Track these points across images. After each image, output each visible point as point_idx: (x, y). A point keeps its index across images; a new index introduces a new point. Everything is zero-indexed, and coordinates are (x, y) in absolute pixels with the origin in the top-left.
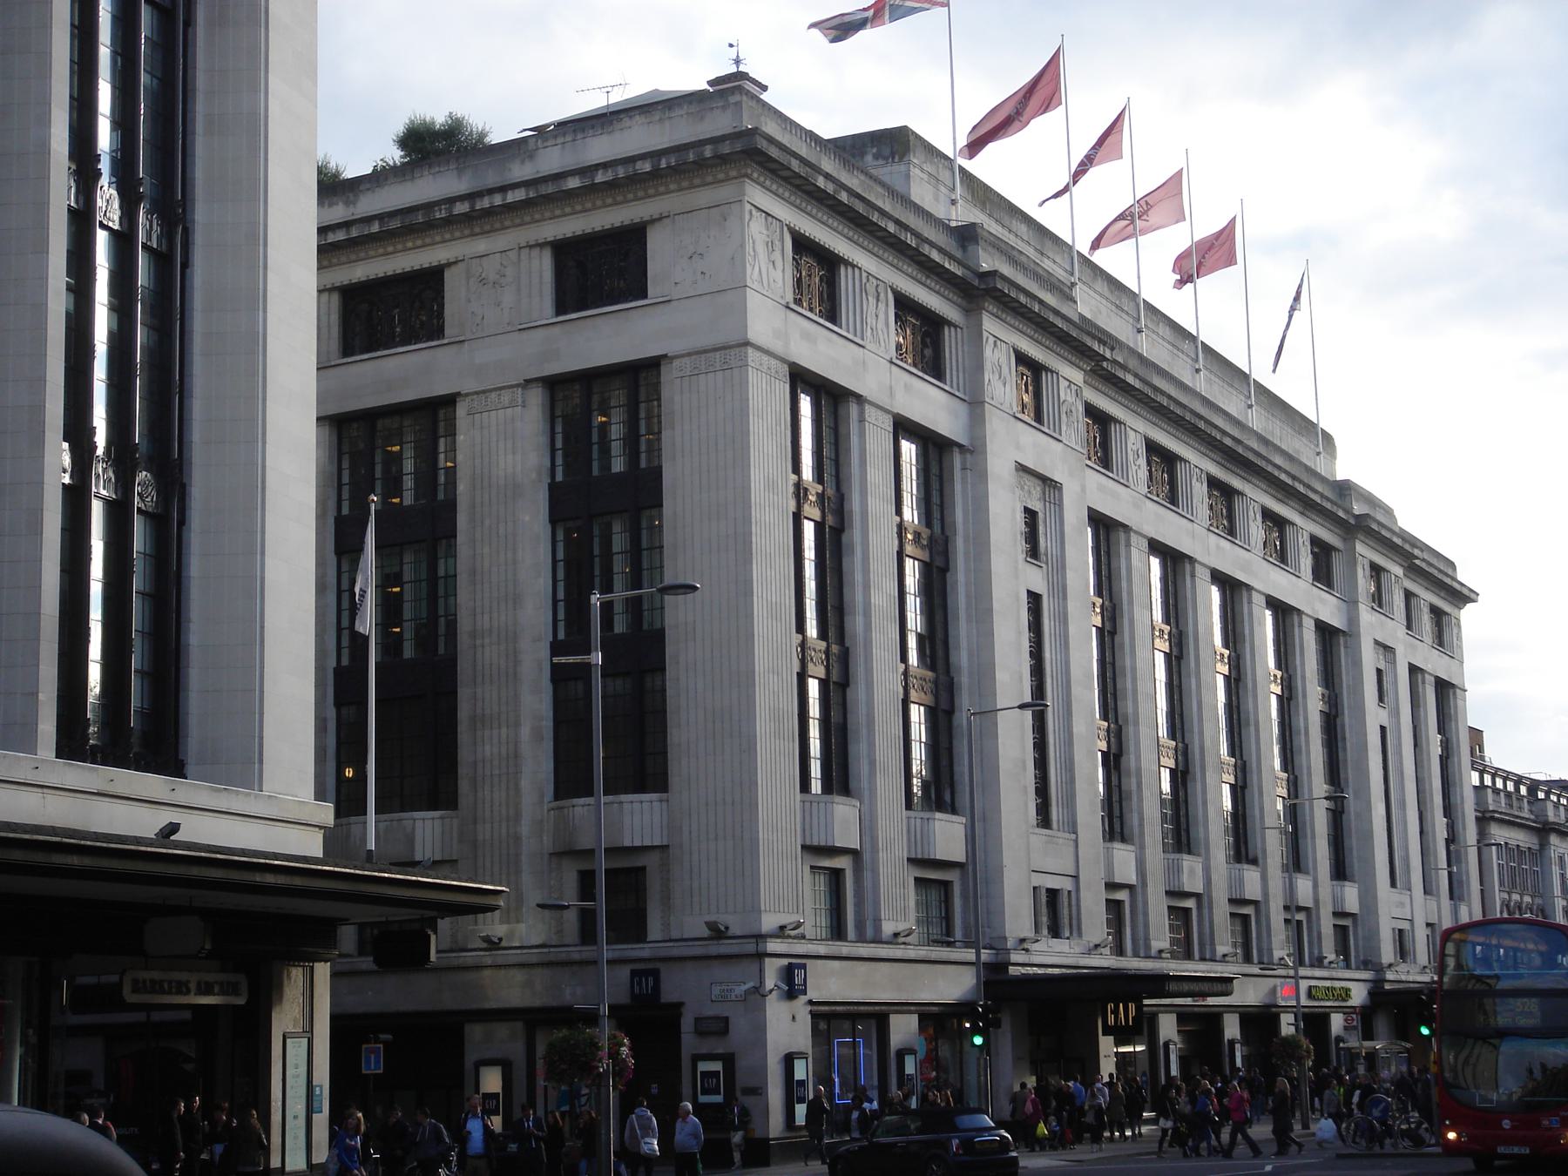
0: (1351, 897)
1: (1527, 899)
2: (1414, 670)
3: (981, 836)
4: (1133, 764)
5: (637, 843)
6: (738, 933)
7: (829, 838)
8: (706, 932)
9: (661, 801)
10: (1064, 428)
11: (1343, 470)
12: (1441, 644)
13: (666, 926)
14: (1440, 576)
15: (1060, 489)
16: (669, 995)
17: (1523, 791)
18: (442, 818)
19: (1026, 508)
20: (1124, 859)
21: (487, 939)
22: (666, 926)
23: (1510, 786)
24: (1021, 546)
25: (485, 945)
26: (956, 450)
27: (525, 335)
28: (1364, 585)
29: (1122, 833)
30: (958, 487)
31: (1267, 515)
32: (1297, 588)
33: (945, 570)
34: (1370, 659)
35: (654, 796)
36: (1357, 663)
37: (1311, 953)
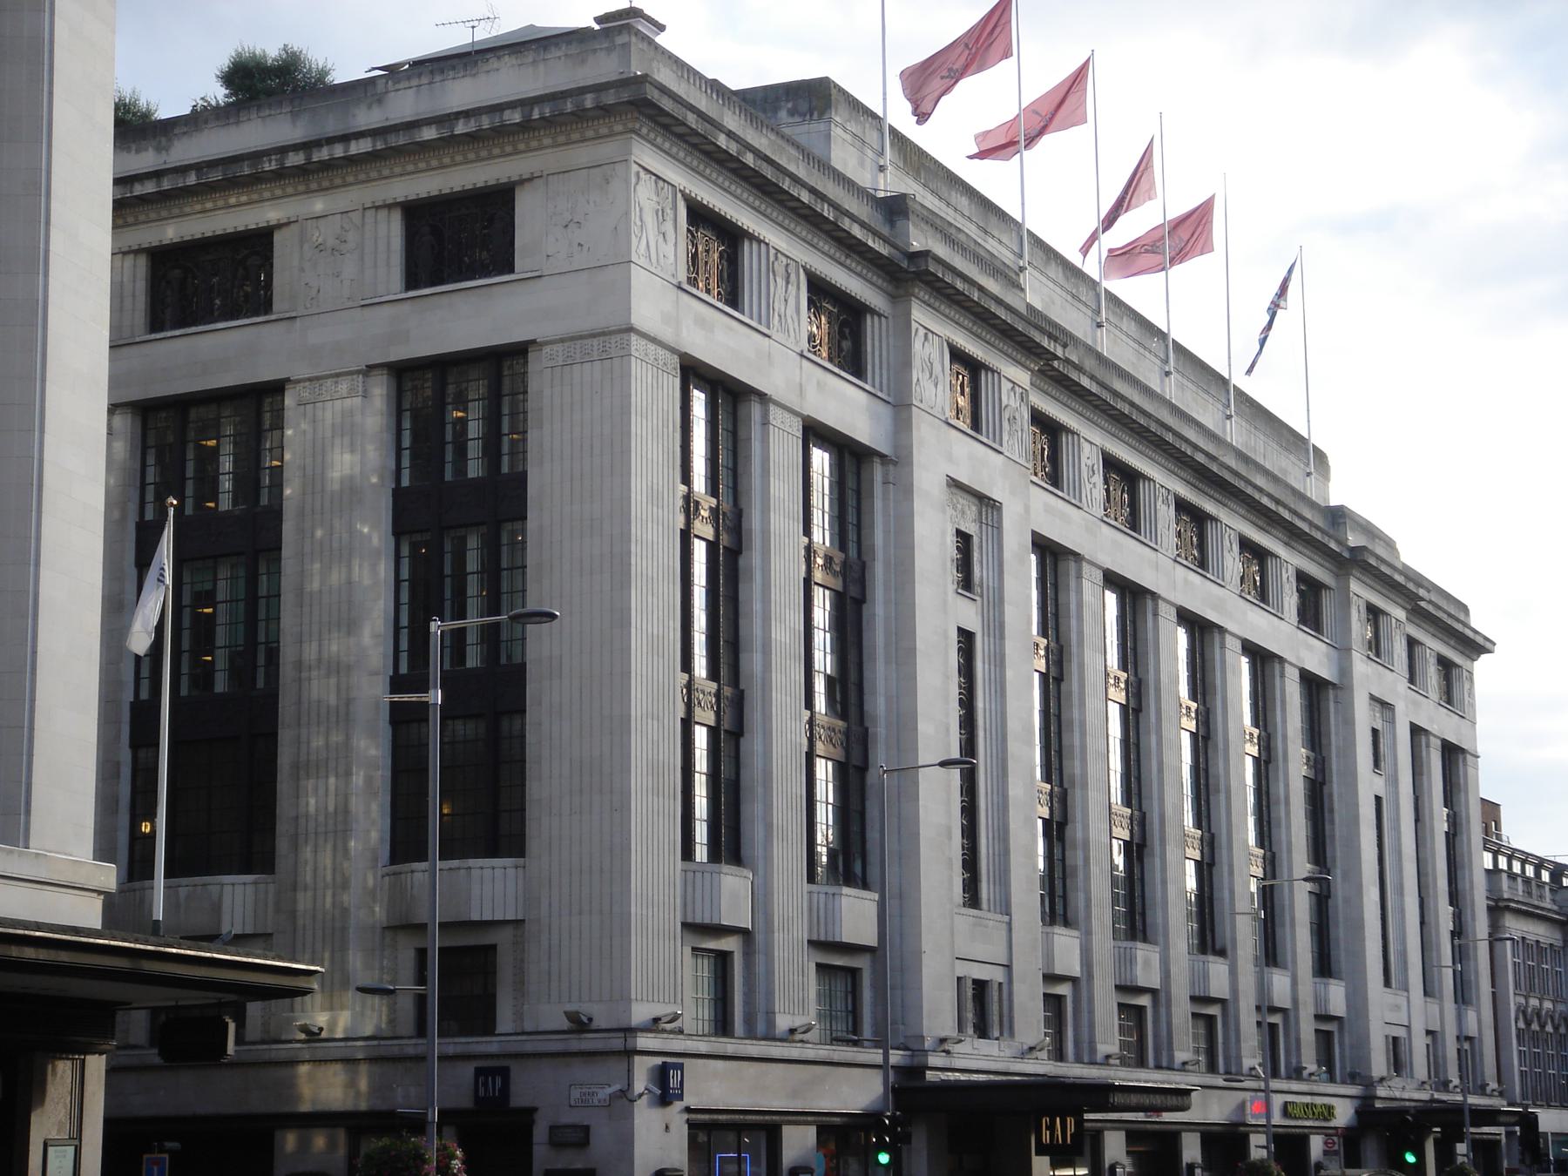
0: (1337, 997)
2: (1416, 730)
3: (1357, 998)
5: (487, 917)
6: (604, 1026)
8: (565, 1024)
9: (516, 867)
10: (1005, 437)
12: (1449, 701)
13: (519, 1015)
14: (1449, 621)
18: (255, 883)
20: (1066, 950)
22: (519, 1015)
23: (1545, 876)
24: (952, 575)
25: (303, 1036)
27: (366, 310)
28: (1359, 629)
30: (878, 504)
33: (861, 601)
34: (1364, 717)
36: (1349, 722)
37: (1343, 1067)
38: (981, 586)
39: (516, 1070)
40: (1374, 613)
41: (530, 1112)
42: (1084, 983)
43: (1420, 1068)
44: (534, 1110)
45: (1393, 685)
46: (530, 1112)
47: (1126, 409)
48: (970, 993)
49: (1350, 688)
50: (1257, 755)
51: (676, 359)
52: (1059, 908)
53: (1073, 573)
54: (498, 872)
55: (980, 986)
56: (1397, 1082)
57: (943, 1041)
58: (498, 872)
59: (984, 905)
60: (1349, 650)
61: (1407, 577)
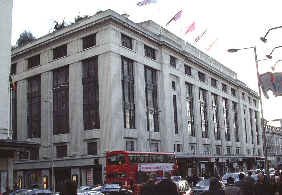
0: (239, 144)
1: (271, 144)
2: (250, 109)
3: (242, 144)
4: (196, 124)
7: (129, 136)
10: (180, 68)
11: (238, 78)
12: (256, 105)
15: (179, 78)
16: (100, 163)
17: (271, 128)
19: (172, 81)
20: (219, 142)
21: (73, 154)
23: (268, 127)
25: (73, 156)
26: (158, 71)
27: (79, 53)
28: (241, 95)
29: (159, 131)
30: (159, 78)
31: (254, 100)
32: (229, 96)
33: (156, 91)
34: (242, 108)
35: (97, 130)
36: (240, 108)
37: (232, 153)
38: (177, 89)
39: (100, 159)
40: (243, 94)
41: (102, 165)
42: (232, 147)
43: (252, 153)
44: (102, 165)
45: (247, 103)
46: (102, 165)
47: (201, 65)
48: (94, 141)
49: (240, 104)
50: (153, 89)
51: (143, 65)
52: (193, 134)
53: (229, 101)
54: (98, 131)
55: (178, 145)
56: (248, 155)
57: (187, 153)
58: (96, 131)
59: (179, 134)
60: (239, 98)
61: (247, 89)
